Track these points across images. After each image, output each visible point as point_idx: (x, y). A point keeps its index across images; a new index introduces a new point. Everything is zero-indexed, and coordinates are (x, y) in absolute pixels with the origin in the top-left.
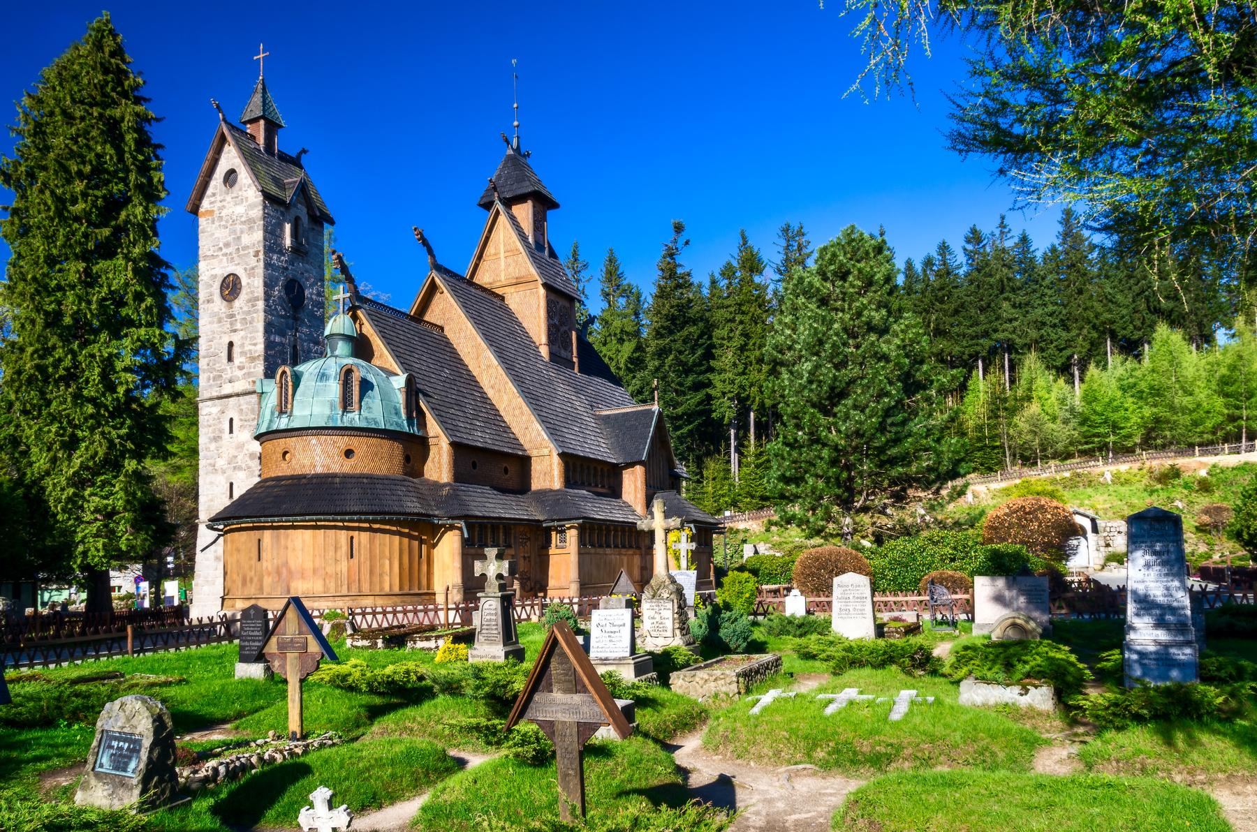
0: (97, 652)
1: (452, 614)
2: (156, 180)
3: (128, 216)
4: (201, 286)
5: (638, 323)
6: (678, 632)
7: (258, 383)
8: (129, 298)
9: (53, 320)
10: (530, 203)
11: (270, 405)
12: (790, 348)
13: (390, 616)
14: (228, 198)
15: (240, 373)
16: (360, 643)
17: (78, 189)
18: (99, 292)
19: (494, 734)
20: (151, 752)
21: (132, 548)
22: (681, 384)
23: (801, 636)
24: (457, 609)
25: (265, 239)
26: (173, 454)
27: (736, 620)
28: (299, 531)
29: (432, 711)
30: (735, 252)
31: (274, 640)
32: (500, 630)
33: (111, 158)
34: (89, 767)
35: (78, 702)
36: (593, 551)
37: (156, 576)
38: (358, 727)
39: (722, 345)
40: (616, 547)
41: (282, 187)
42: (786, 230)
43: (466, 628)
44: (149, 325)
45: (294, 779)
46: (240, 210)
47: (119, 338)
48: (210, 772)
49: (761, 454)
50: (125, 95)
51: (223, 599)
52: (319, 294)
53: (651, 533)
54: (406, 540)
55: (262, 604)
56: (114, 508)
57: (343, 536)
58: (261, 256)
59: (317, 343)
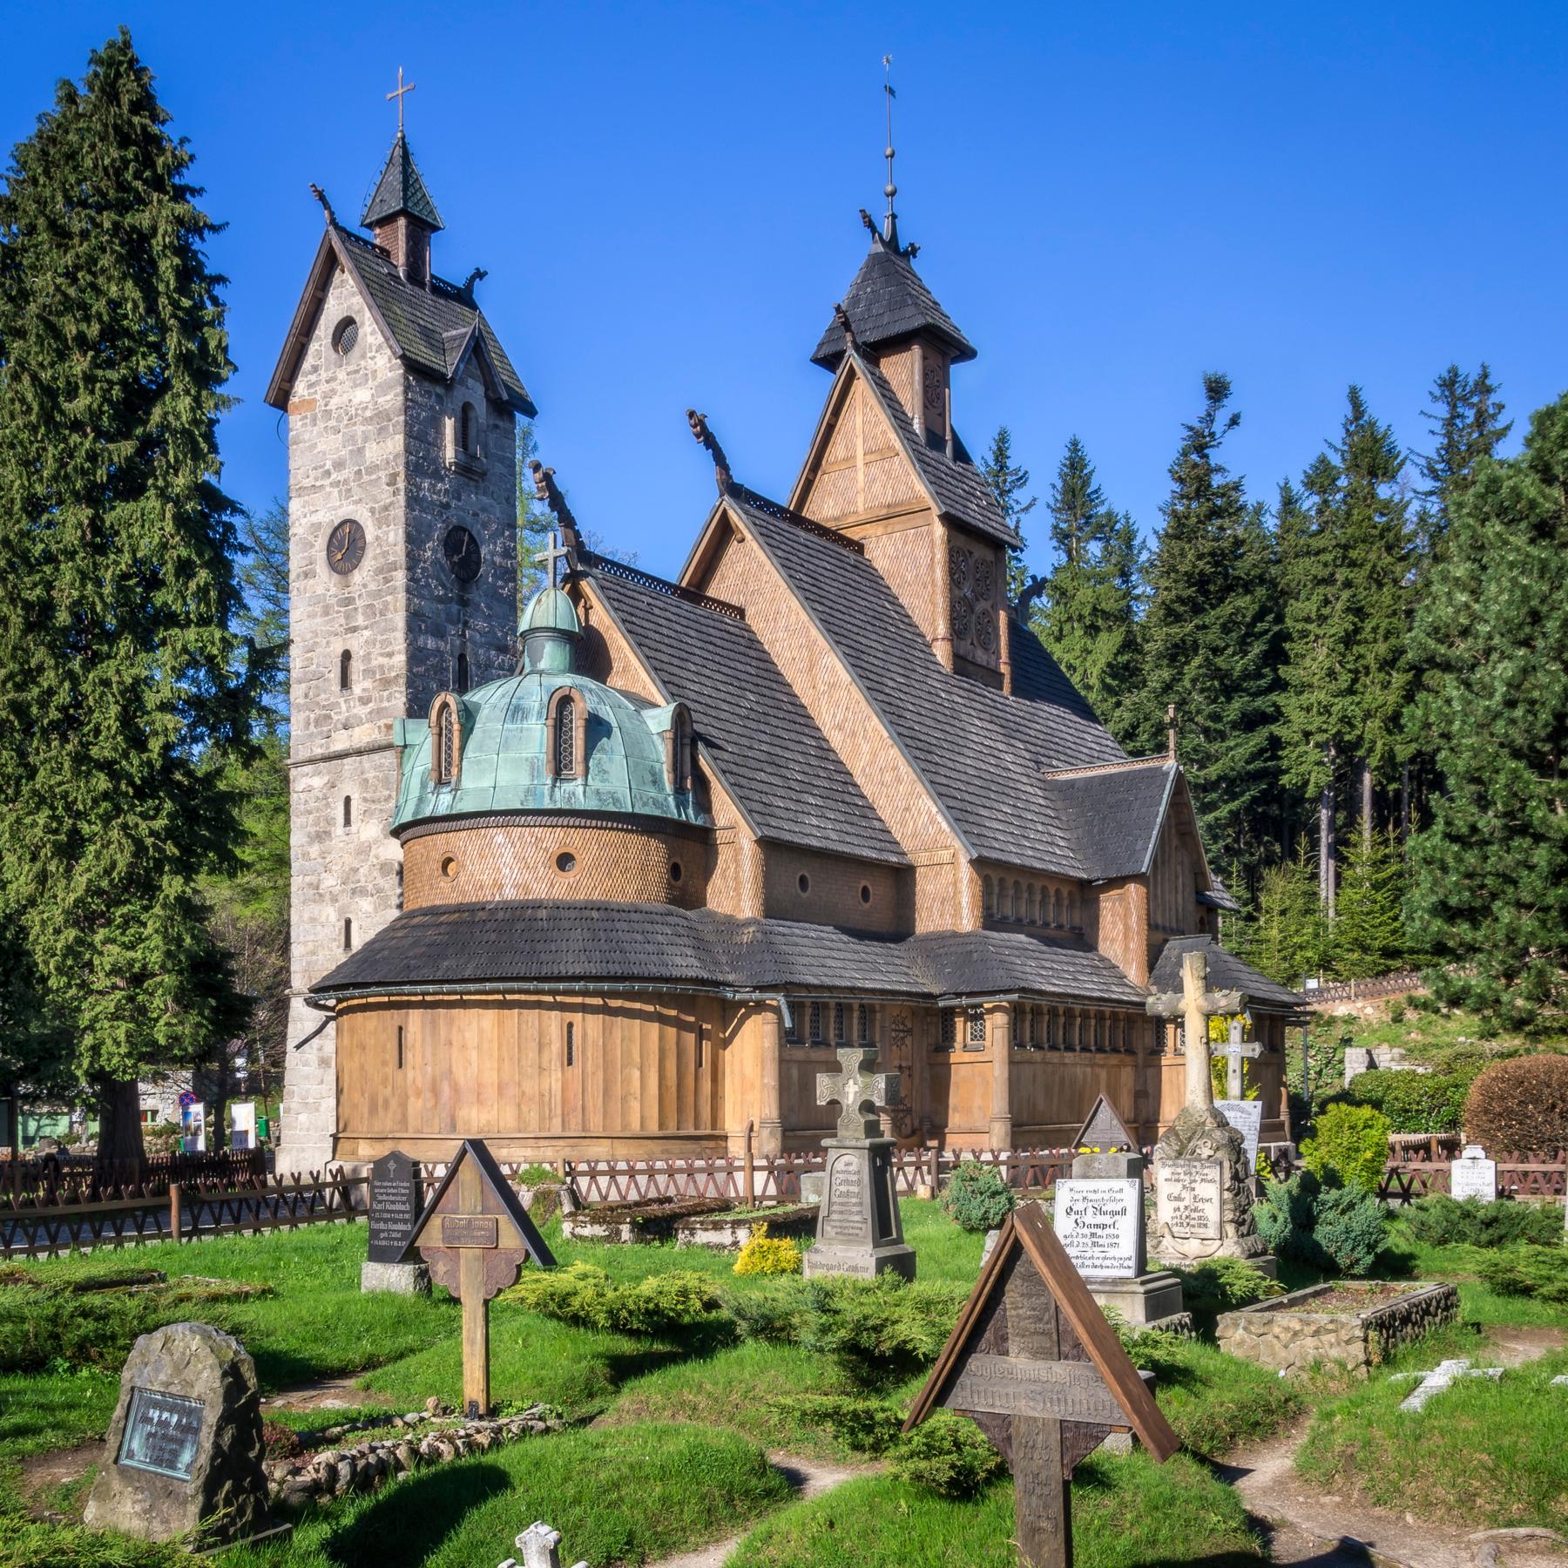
0: (119, 1233)
1: (760, 1177)
2: (212, 344)
3: (166, 414)
4: (293, 547)
5: (1127, 594)
6: (1230, 1229)
7: (397, 727)
8: (168, 572)
9: (39, 616)
10: (916, 350)
11: (419, 770)
12: (1465, 632)
13: (642, 1180)
14: (341, 375)
15: (362, 711)
16: (587, 1231)
17: (78, 370)
18: (116, 563)
19: (869, 1430)
20: (218, 1434)
21: (176, 1039)
22: (1216, 717)
23: (1491, 1244)
24: (770, 1169)
25: (408, 450)
26: (247, 866)
27: (1351, 1206)
28: (473, 1012)
29: (735, 1372)
30: (1337, 436)
31: (436, 1221)
32: (868, 1214)
33: (136, 307)
34: (108, 1455)
35: (88, 1327)
36: (1038, 1056)
37: (217, 1092)
38: (591, 1396)
39: (1304, 634)
40: (1085, 1049)
41: (440, 348)
42: (1449, 383)
43: (791, 1207)
44: (204, 621)
45: (479, 1498)
46: (363, 395)
47: (150, 648)
48: (323, 1474)
49: (1384, 860)
50: (158, 184)
51: (336, 1139)
52: (509, 553)
53: (1178, 1020)
54: (671, 1032)
55: (410, 1151)
56: (144, 966)
57: (554, 1022)
58: (401, 484)
59: (503, 649)
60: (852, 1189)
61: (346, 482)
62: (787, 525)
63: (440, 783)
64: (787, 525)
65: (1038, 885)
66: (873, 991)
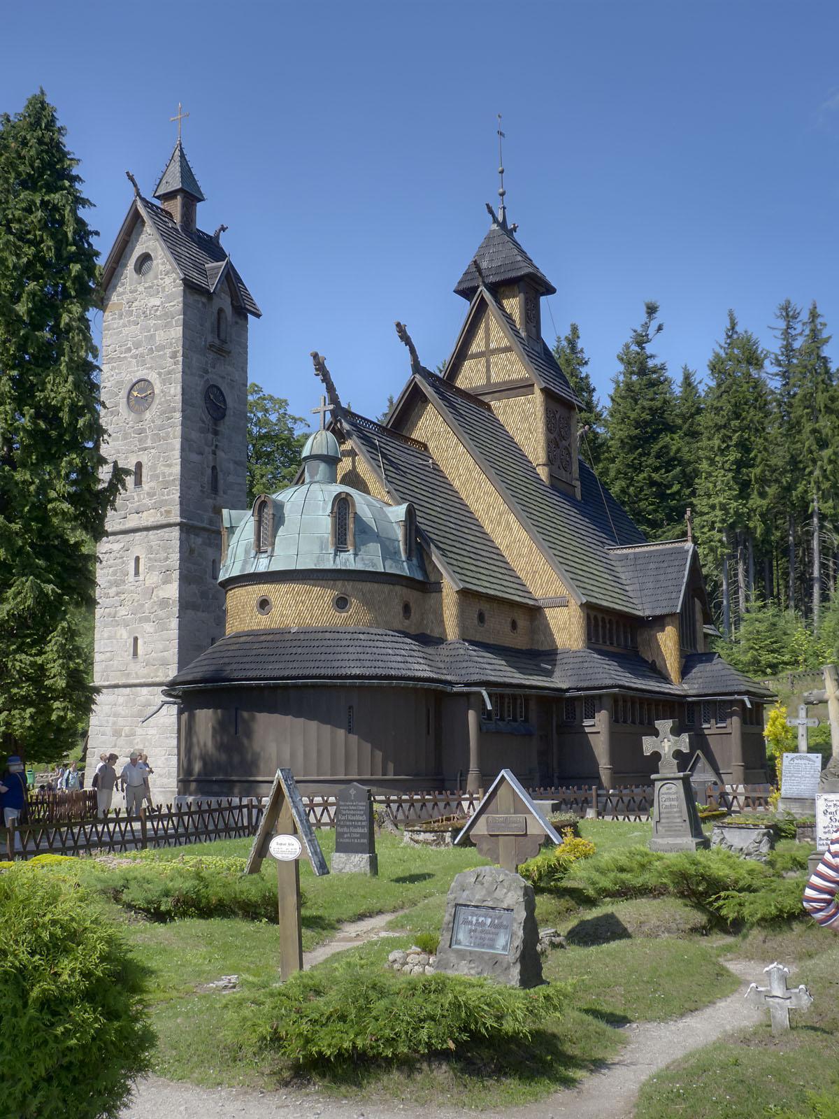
11: (243, 543)
14: (141, 289)
15: (147, 501)
16: (422, 837)
41: (203, 272)
46: (155, 301)
60: (673, 803)
61: (142, 356)
63: (259, 551)
66: (637, 689)
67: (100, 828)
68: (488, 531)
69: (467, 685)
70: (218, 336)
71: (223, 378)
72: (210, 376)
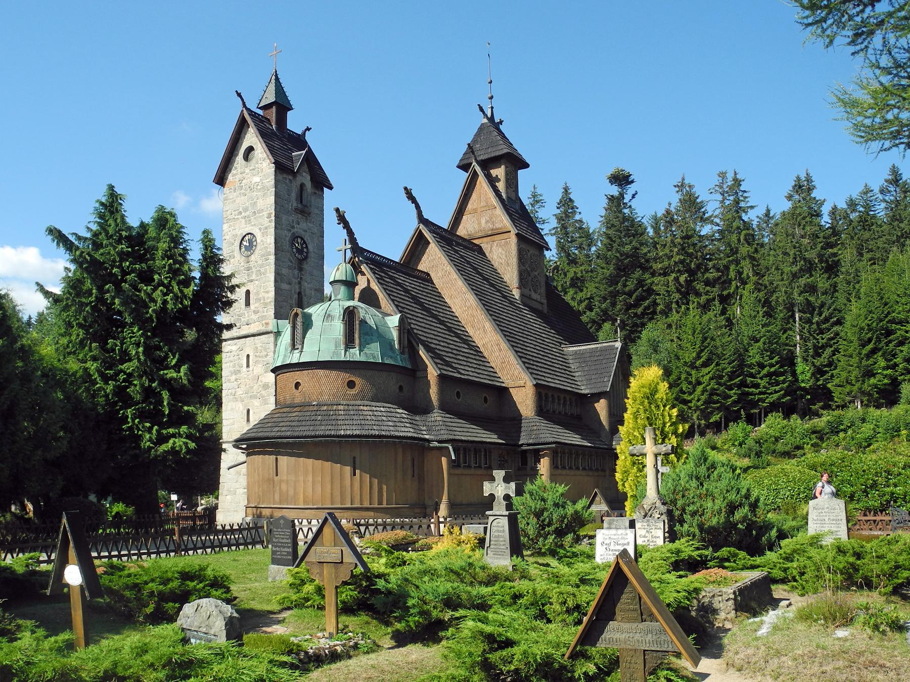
14: (247, 171)
15: (254, 317)
41: (291, 159)
46: (256, 179)
61: (249, 217)
62: (449, 239)
63: (294, 347)
64: (449, 239)
65: (562, 396)
67: (203, 538)
68: (471, 334)
69: (439, 442)
70: (301, 202)
71: (306, 231)
72: (295, 230)
